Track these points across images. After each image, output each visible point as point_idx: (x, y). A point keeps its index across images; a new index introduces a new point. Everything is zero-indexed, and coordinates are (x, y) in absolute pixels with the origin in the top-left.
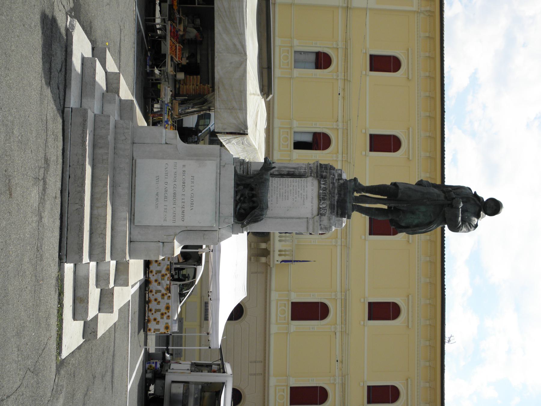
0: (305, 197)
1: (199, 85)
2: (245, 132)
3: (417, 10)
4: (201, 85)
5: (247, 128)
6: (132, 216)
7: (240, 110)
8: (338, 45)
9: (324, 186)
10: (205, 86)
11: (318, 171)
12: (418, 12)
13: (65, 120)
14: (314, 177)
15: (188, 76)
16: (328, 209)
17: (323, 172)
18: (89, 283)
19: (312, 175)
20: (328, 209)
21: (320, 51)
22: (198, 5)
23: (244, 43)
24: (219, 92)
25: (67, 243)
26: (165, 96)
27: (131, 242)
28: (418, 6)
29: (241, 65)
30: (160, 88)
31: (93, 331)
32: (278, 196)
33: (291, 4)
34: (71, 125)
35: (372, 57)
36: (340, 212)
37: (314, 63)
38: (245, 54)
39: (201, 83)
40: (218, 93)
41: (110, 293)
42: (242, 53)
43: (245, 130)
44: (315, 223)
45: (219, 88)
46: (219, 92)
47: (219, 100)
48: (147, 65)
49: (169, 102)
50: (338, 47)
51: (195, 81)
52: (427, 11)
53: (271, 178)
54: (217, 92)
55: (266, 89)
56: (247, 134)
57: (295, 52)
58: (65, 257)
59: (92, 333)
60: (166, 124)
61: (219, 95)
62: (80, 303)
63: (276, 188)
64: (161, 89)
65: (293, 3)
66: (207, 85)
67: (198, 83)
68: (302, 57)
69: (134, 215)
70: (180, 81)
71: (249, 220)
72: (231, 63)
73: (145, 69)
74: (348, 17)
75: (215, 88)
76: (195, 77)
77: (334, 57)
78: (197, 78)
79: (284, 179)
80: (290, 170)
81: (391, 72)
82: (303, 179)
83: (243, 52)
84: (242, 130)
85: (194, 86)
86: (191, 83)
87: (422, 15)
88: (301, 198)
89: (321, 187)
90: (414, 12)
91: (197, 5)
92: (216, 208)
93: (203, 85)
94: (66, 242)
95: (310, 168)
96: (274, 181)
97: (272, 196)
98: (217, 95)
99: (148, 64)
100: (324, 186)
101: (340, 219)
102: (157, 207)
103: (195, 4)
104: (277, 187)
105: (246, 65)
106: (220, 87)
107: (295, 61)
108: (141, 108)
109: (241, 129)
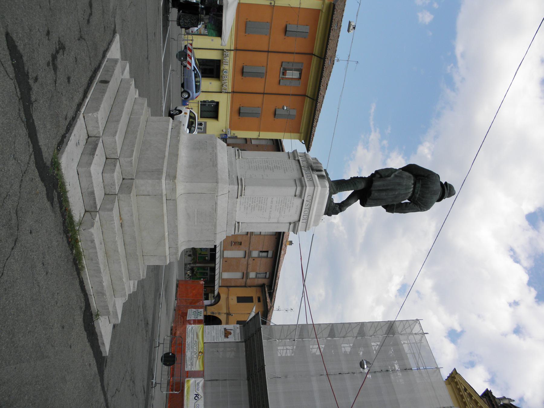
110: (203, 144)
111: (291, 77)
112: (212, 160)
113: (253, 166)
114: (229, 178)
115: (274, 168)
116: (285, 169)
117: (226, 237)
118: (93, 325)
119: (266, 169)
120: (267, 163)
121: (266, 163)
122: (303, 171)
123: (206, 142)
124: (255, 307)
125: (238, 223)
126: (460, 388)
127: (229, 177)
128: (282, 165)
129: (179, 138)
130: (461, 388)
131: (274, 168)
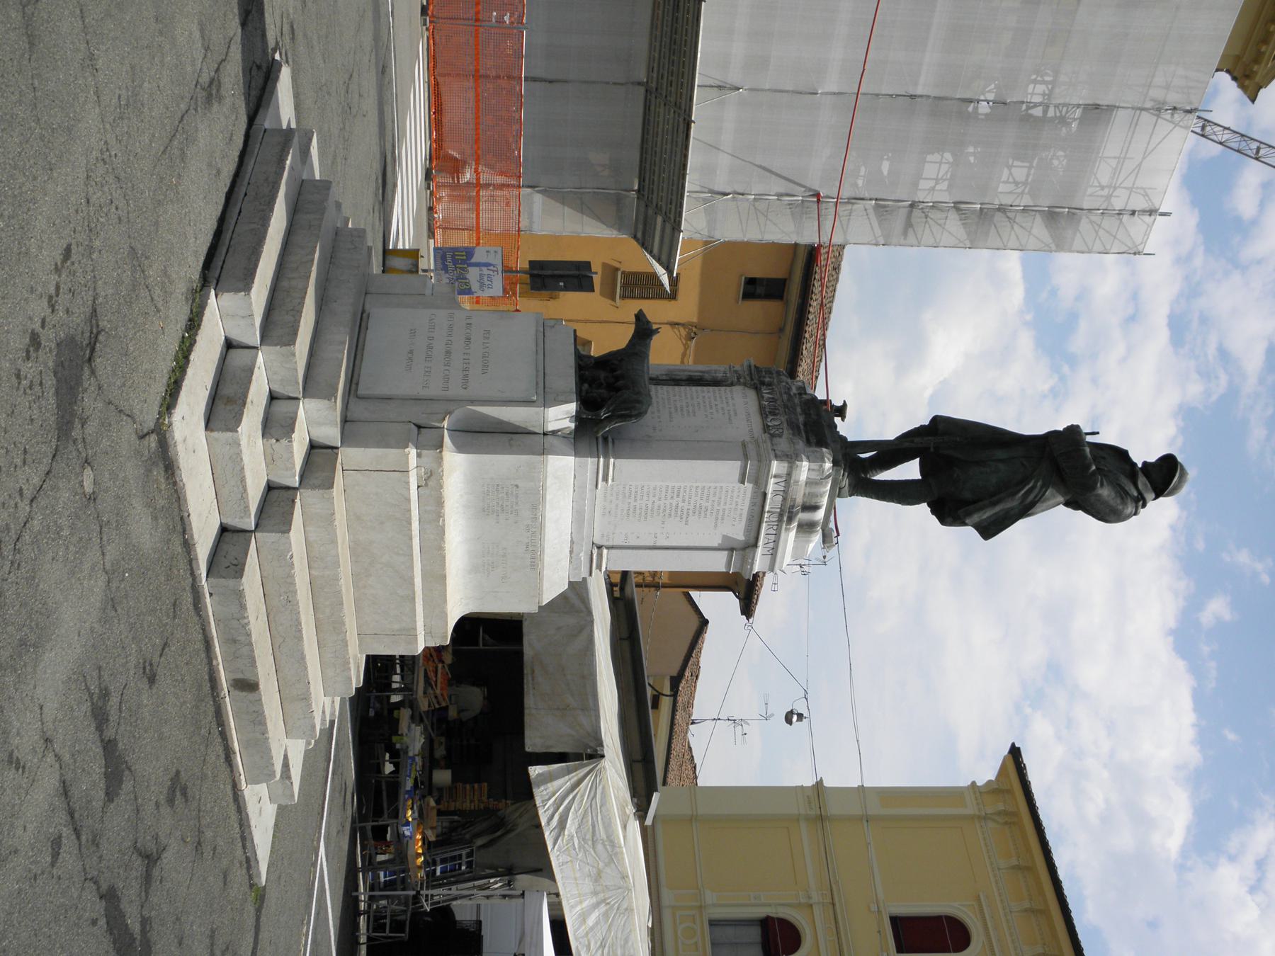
0: (732, 413)
1: (486, 801)
2: (596, 751)
3: (977, 813)
4: (491, 800)
5: (601, 745)
6: (354, 386)
7: (582, 710)
8: (810, 898)
9: (771, 396)
10: (500, 804)
11: (753, 371)
12: (979, 817)
13: (251, 134)
14: (745, 385)
15: (461, 785)
16: (785, 428)
17: (764, 377)
18: (252, 376)
19: (742, 380)
20: (785, 428)
21: (771, 915)
22: (484, 645)
23: (585, 595)
24: (533, 680)
25: (222, 268)
26: (409, 730)
27: (346, 421)
28: (978, 804)
29: (581, 630)
30: (399, 716)
31: (235, 562)
32: (673, 410)
33: (691, 820)
34: (261, 143)
35: (896, 921)
36: (813, 440)
37: (760, 946)
38: (590, 613)
39: (488, 798)
40: (531, 682)
41: (288, 499)
42: (582, 612)
43: (598, 748)
44: (761, 445)
45: (533, 672)
46: (533, 680)
47: (534, 695)
48: (359, 914)
49: (417, 752)
50: (811, 902)
51: (476, 793)
52: (999, 813)
53: (653, 388)
54: (530, 678)
55: (641, 784)
56: (603, 756)
57: (713, 923)
58: (215, 281)
59: (232, 567)
60: (408, 799)
61: (533, 684)
62: (225, 404)
63: (666, 401)
64: (401, 717)
65: (695, 813)
66: (504, 801)
67: (485, 798)
68: (730, 932)
69: (357, 384)
70: (440, 789)
71: (611, 409)
72: (559, 629)
73: (368, 694)
74: (823, 848)
75: (525, 672)
76: (476, 786)
77: (803, 922)
78: (481, 789)
79: (682, 388)
80: (692, 374)
81: (949, 951)
82: (723, 388)
83: (584, 610)
84: (590, 747)
85: (473, 804)
86: (468, 797)
87: (991, 824)
88: (724, 414)
89: (763, 397)
90: (972, 817)
91: (481, 647)
92: (537, 376)
93: (494, 801)
94: (223, 258)
95: (736, 372)
96: (660, 391)
97: (659, 411)
98: (530, 685)
99: (372, 705)
100: (771, 396)
101: (818, 449)
102: (409, 368)
103: (477, 644)
104: (669, 399)
105: (592, 631)
106: (536, 671)
107: (713, 944)
108: (356, 718)
109: (587, 746)
110: (507, 494)
111: (767, 508)
112: (531, 549)
113: (638, 507)
114: (571, 562)
115: (691, 513)
116: (721, 513)
117: (567, 587)
118: (325, 399)
119: (670, 515)
120: (678, 496)
121: (675, 496)
122: (764, 526)
123: (517, 486)
124: (668, 289)
125: (599, 547)
126: (1263, 54)
127: (571, 557)
128: (716, 504)
129: (444, 520)
130: (1267, 54)
131: (691, 513)
